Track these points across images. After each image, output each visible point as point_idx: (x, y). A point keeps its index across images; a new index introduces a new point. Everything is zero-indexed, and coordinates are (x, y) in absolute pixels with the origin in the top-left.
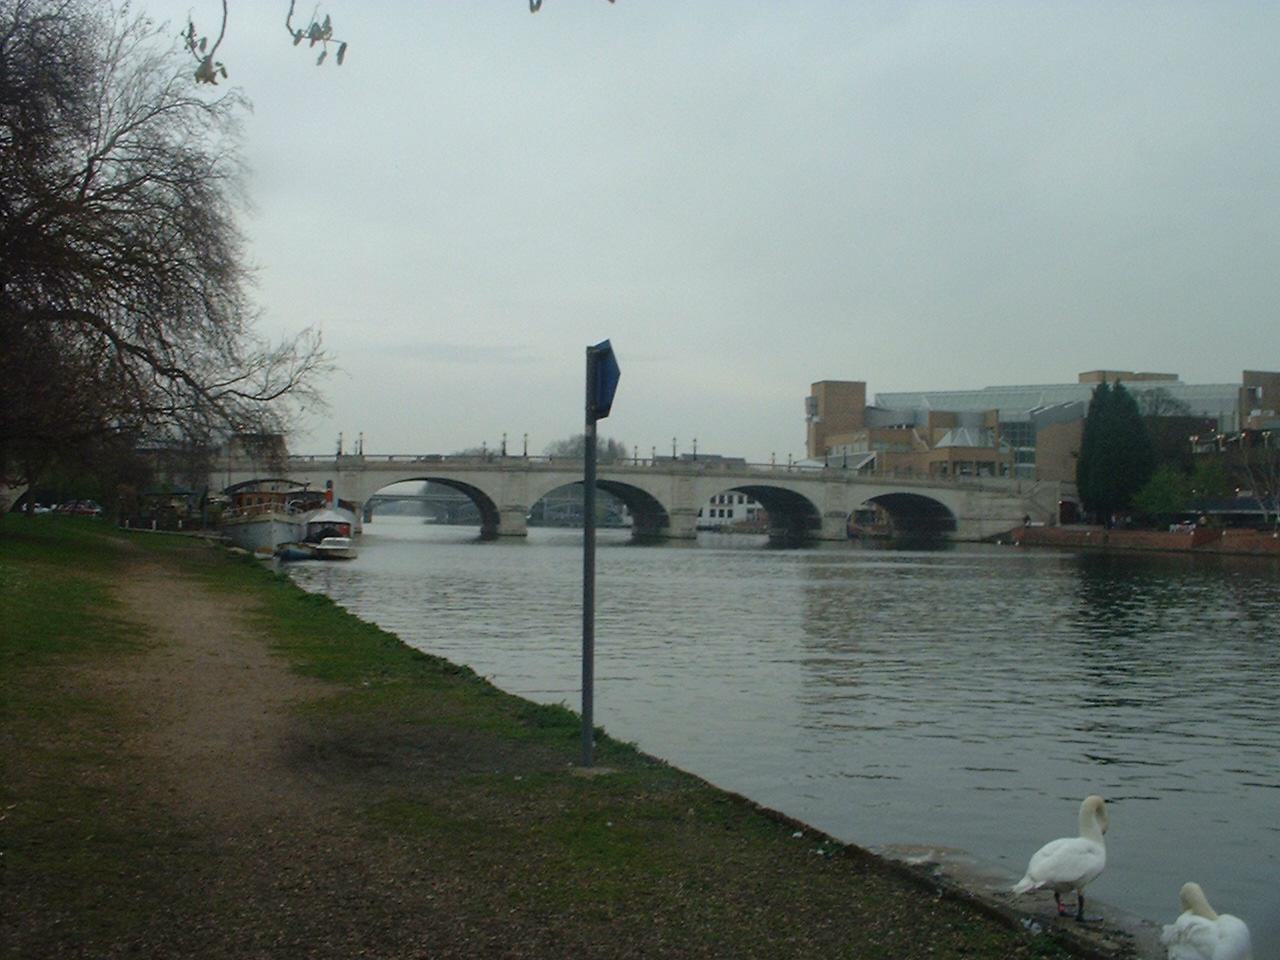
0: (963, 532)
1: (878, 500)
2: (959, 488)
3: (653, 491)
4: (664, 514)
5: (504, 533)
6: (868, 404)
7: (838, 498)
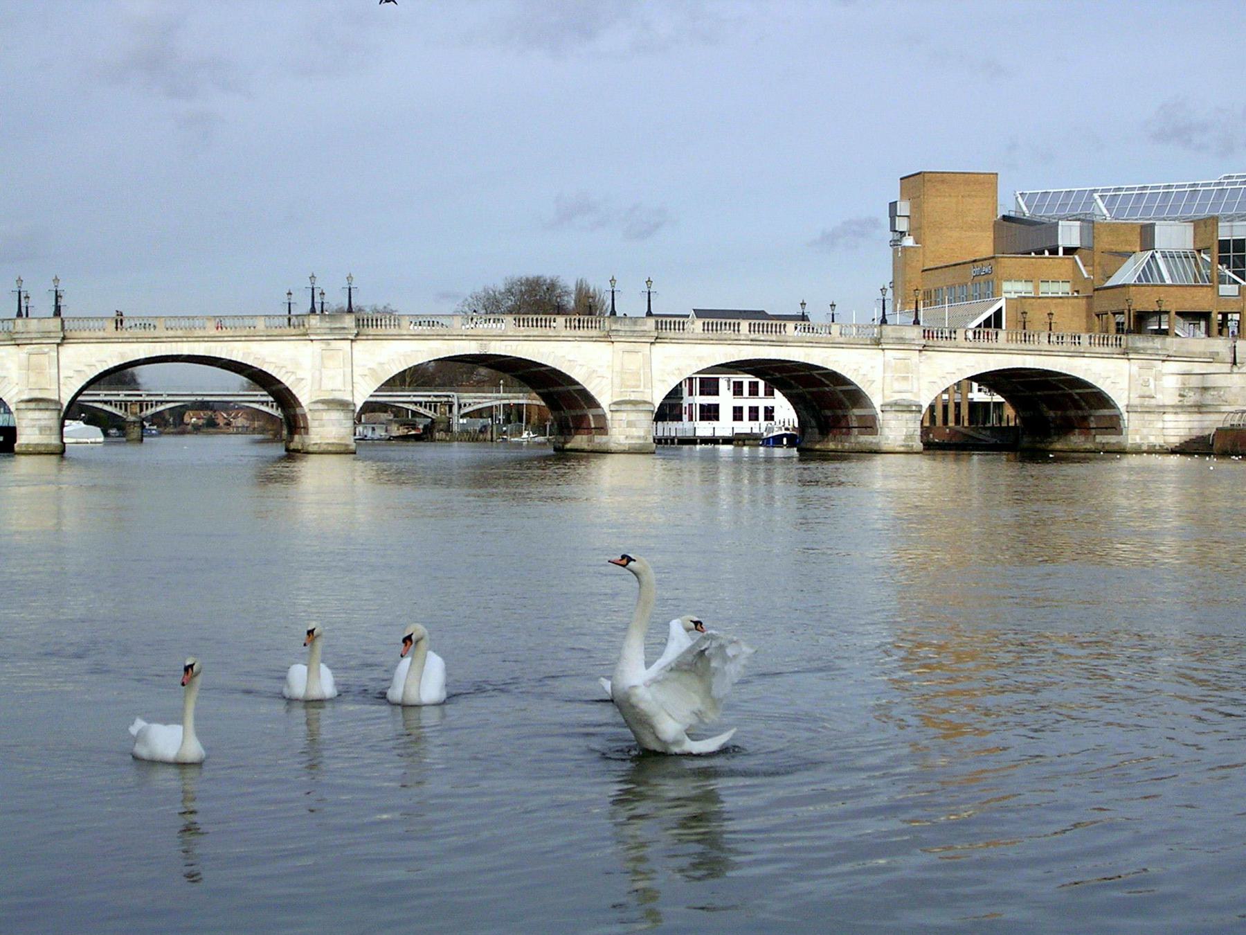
0: (1137, 431)
1: (988, 380)
4: (599, 411)
5: (315, 448)
7: (905, 378)
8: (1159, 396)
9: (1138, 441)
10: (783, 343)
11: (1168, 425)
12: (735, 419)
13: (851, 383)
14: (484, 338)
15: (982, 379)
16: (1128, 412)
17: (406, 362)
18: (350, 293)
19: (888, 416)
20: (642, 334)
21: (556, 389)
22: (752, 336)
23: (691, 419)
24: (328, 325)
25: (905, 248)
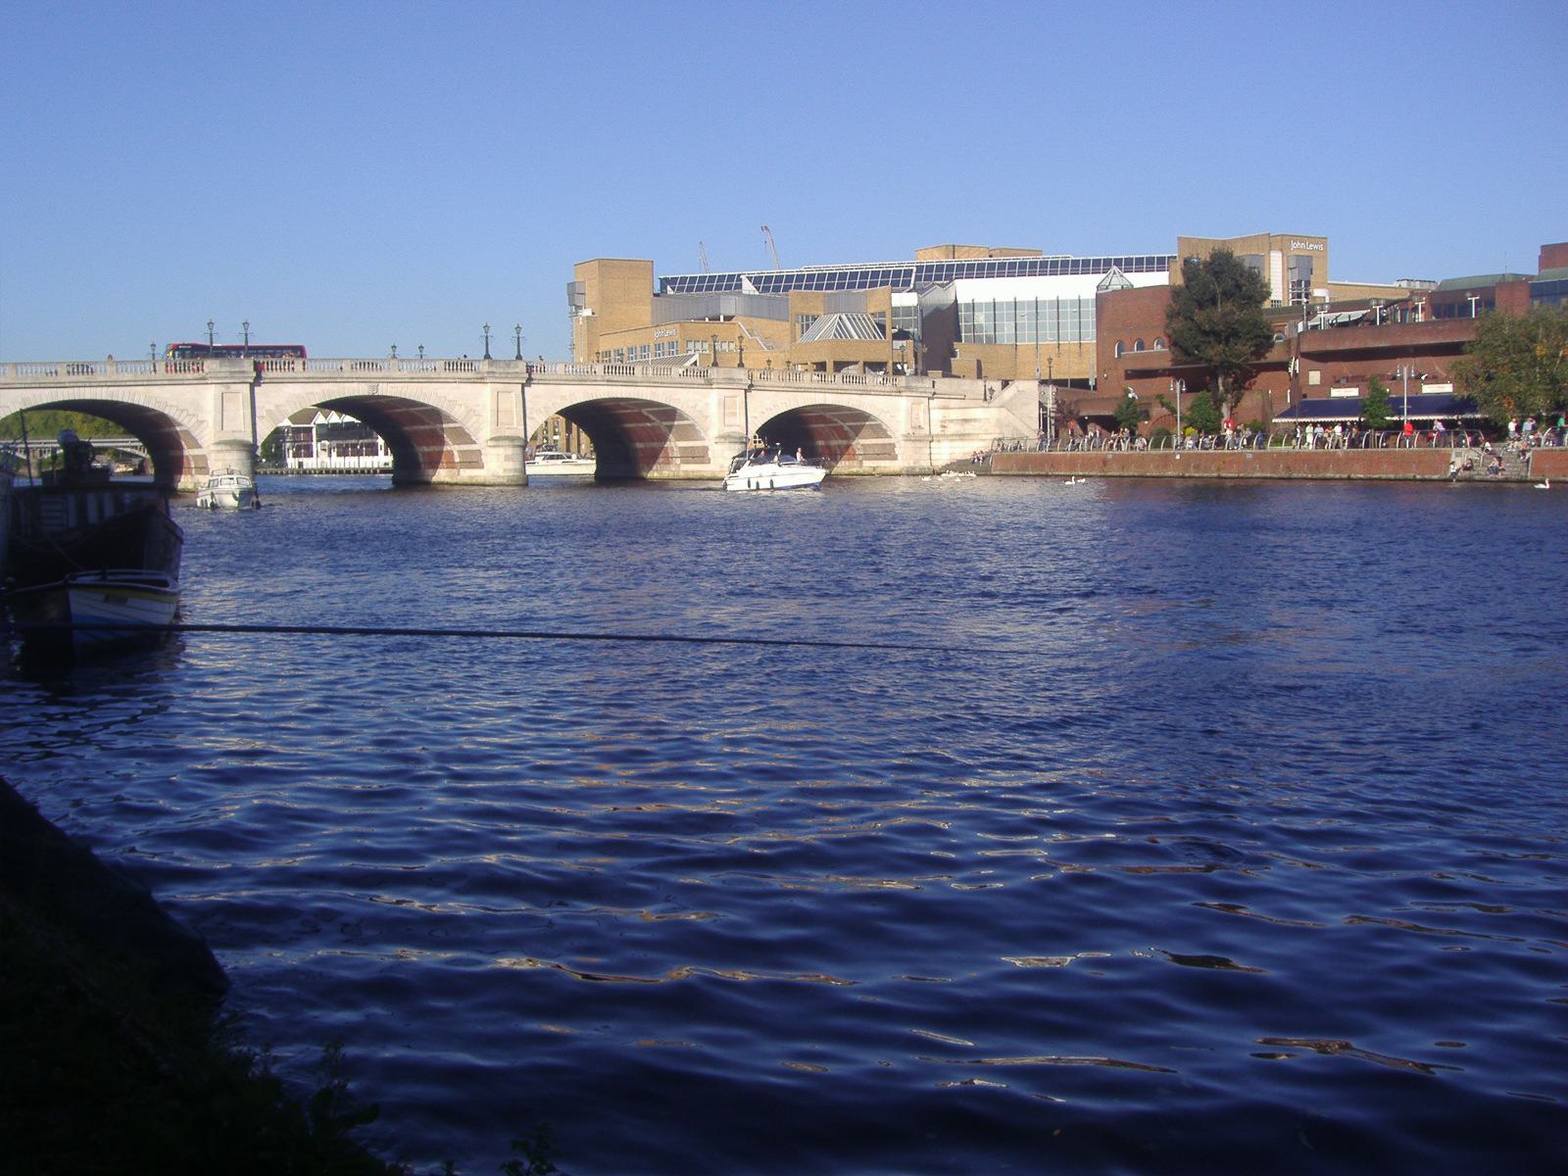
9: (912, 465)
10: (634, 384)
15: (328, 406)
17: (300, 403)
20: (514, 375)
21: (415, 427)
22: (607, 377)
24: (228, 369)
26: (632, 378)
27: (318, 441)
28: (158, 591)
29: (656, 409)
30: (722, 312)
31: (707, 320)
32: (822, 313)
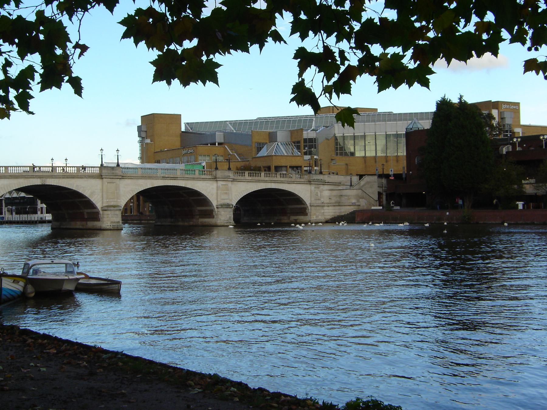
0: (315, 215)
2: (309, 182)
3: (87, 193)
4: (95, 210)
6: (182, 131)
7: (226, 193)
8: (322, 199)
11: (325, 211)
12: (41, 214)
13: (86, 197)
14: (44, 177)
15: (19, 190)
16: (311, 206)
18: (102, 157)
19: (220, 210)
23: (42, 213)
25: (147, 144)
26: (194, 176)
27: (5, 206)
28: (287, 231)
29: (187, 191)
30: (217, 141)
31: (209, 145)
32: (268, 142)
